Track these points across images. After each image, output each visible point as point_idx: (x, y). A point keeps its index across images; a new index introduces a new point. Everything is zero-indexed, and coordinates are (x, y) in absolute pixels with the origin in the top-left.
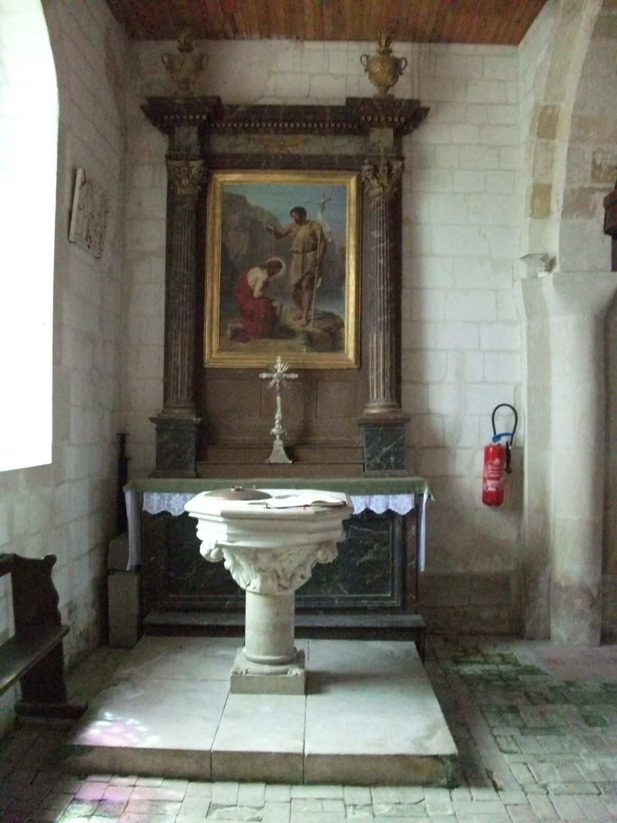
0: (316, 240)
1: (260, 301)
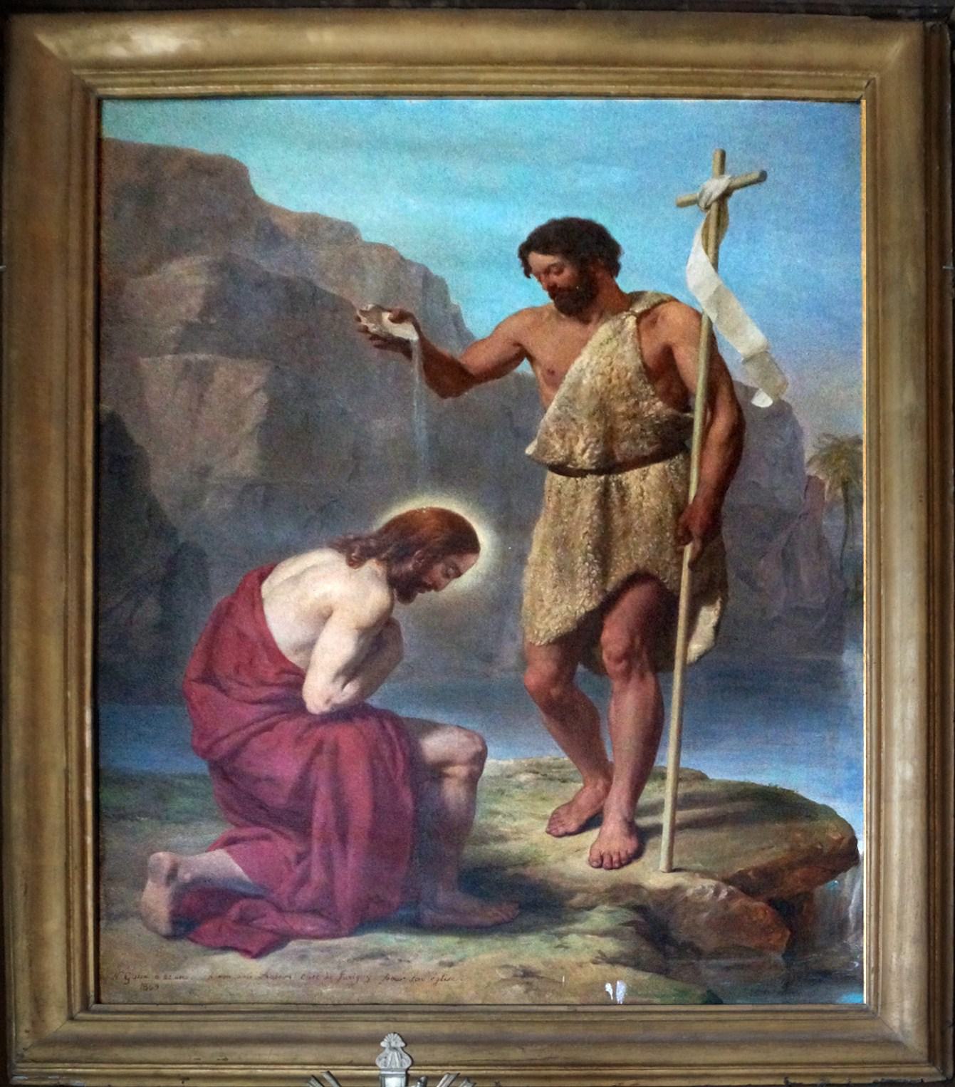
0: (682, 399)
1: (346, 736)
